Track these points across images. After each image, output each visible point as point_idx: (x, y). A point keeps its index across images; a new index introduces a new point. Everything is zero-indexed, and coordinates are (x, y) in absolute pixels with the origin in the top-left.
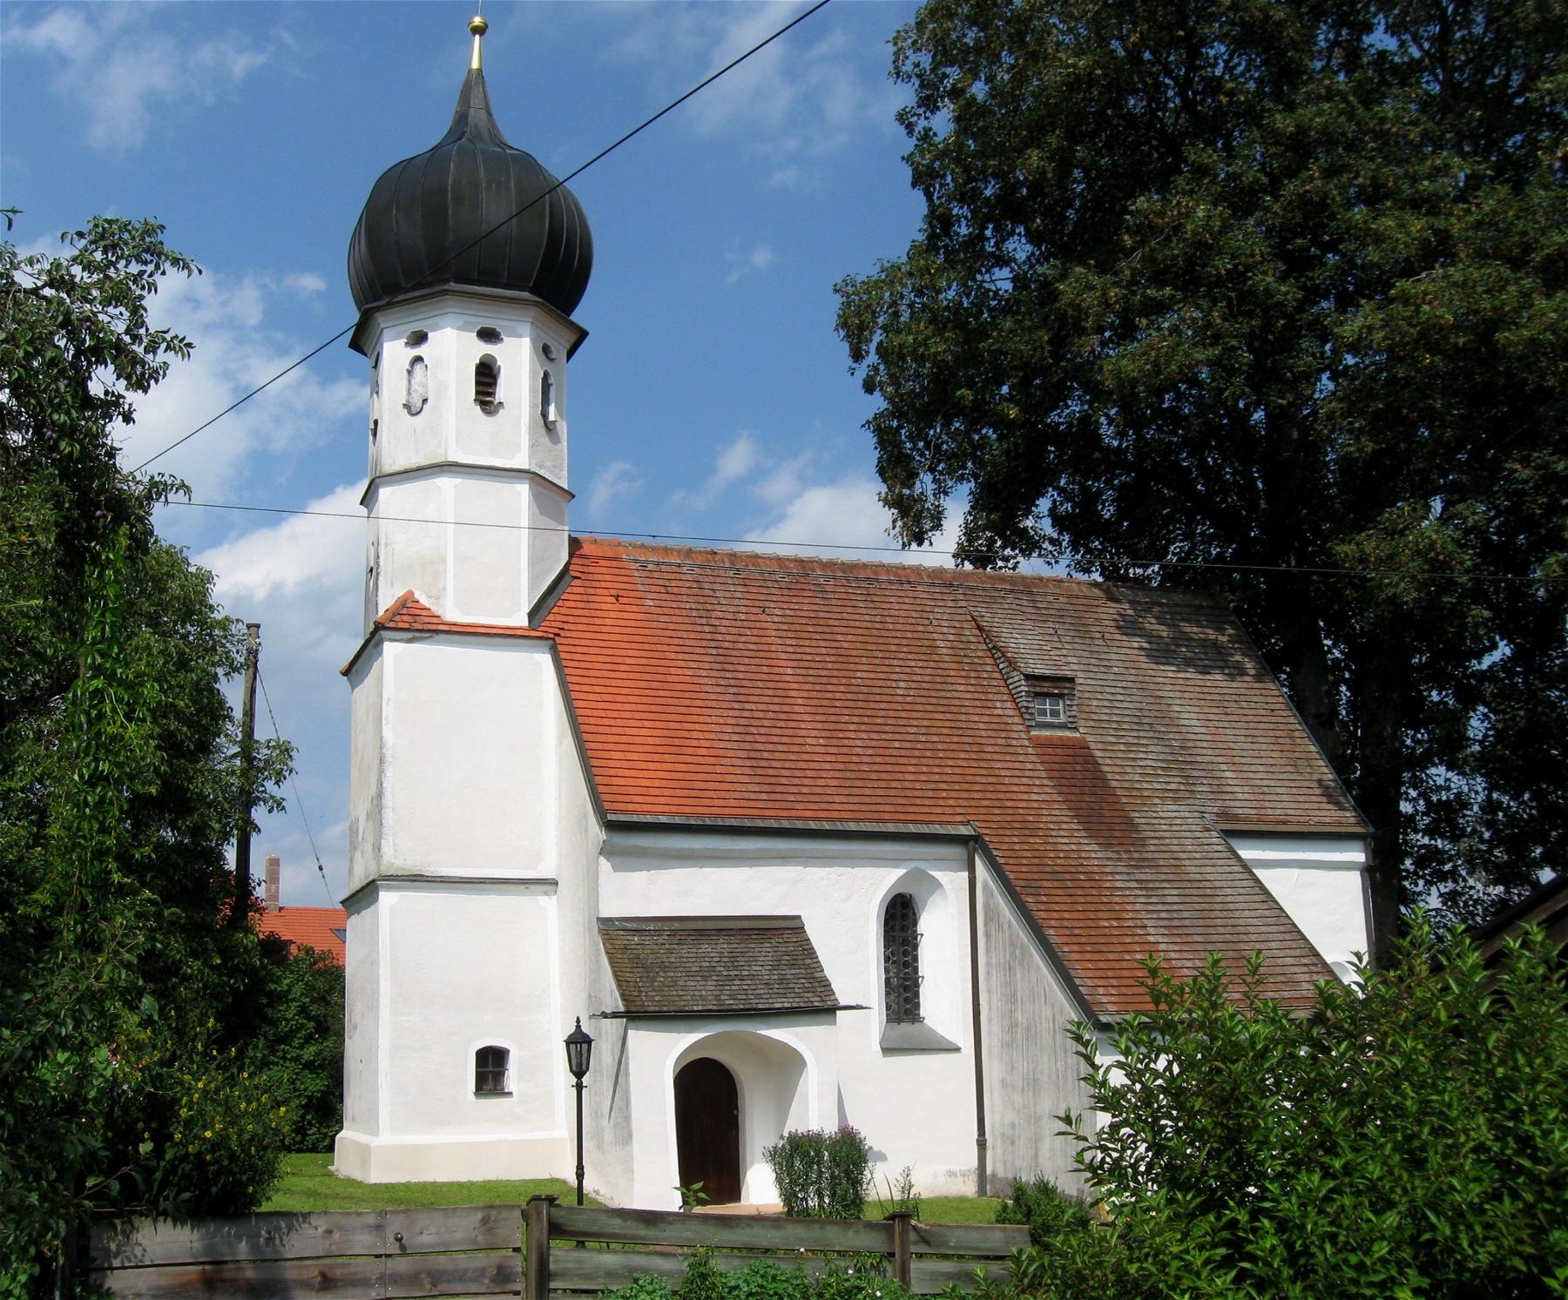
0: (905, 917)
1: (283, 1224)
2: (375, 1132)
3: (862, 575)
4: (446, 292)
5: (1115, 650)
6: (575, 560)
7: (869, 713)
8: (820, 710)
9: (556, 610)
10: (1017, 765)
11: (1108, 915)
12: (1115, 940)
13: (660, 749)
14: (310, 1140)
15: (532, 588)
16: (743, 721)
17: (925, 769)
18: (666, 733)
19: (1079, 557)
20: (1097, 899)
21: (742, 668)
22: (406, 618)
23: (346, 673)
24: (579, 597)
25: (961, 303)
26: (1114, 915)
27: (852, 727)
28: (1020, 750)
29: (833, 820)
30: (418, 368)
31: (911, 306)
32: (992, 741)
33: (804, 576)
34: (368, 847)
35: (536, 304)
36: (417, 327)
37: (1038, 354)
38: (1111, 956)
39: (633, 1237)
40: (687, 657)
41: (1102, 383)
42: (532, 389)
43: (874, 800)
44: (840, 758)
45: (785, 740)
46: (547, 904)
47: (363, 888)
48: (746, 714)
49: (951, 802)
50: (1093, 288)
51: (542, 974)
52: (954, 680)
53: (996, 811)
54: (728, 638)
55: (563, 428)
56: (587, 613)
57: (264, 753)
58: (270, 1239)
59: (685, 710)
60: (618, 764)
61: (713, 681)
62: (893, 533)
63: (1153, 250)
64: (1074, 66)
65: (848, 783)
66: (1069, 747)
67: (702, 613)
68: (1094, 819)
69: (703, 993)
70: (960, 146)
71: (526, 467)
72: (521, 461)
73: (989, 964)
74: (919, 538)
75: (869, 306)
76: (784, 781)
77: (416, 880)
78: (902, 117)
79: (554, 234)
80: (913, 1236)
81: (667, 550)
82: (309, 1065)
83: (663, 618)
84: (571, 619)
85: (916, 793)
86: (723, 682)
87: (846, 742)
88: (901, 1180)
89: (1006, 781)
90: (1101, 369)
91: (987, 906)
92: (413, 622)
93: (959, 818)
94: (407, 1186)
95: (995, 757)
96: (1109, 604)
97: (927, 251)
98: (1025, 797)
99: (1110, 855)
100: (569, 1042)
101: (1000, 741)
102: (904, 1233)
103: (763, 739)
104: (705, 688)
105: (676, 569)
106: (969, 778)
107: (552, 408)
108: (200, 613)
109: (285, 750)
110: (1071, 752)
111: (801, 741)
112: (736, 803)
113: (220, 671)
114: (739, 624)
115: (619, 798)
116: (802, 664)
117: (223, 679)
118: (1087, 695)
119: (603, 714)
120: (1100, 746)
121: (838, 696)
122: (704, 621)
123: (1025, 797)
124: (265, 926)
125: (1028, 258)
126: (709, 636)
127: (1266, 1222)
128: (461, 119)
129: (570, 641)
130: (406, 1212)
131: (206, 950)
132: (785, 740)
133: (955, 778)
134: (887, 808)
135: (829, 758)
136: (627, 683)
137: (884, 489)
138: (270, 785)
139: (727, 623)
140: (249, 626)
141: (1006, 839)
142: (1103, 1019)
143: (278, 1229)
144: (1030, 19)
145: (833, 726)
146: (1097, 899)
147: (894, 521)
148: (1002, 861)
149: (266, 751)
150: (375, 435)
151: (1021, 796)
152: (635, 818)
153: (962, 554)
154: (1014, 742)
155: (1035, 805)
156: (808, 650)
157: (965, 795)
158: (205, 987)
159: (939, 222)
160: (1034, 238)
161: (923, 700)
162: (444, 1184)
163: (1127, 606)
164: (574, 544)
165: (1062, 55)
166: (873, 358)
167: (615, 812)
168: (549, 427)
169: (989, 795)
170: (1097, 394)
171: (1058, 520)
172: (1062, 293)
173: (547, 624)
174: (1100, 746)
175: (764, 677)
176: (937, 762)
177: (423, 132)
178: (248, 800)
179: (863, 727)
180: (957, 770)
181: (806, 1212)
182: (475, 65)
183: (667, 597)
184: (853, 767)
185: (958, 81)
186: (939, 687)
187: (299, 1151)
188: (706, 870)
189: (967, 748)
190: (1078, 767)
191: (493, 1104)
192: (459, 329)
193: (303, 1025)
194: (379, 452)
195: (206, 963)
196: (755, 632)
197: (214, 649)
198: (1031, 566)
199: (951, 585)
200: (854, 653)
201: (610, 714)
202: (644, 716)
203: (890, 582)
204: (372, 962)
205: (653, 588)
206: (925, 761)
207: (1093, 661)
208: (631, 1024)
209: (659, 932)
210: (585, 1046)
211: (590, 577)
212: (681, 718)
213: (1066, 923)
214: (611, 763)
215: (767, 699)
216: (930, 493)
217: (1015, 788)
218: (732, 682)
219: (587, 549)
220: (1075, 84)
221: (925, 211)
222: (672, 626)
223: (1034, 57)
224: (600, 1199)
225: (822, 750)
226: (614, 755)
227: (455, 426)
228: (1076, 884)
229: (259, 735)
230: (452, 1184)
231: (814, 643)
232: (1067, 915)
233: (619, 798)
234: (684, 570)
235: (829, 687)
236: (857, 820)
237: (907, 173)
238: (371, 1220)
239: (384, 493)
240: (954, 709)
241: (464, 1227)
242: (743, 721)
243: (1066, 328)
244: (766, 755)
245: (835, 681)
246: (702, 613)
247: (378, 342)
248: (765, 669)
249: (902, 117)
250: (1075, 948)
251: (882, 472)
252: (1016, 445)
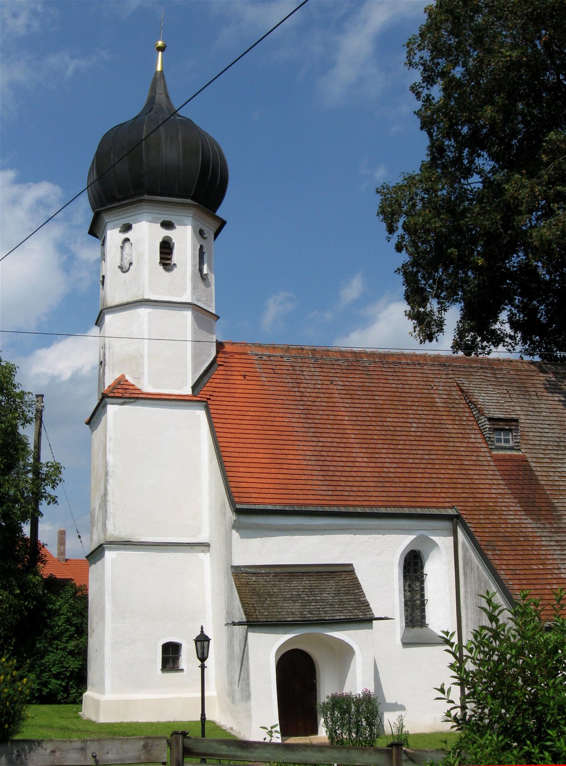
0: (416, 564)
1: (26, 747)
2: (102, 692)
3: (391, 360)
4: (141, 201)
5: (544, 402)
6: (220, 355)
7: (394, 442)
8: (365, 441)
9: (208, 384)
10: (484, 472)
11: (537, 562)
12: (541, 577)
13: (268, 466)
14: (71, 699)
15: (194, 372)
16: (318, 449)
17: (427, 475)
18: (273, 456)
19: (527, 347)
20: (531, 552)
21: (318, 417)
22: (120, 391)
23: (88, 423)
24: (222, 377)
25: (450, 198)
26: (540, 562)
27: (384, 451)
28: (485, 463)
29: (371, 506)
30: (127, 245)
31: (422, 199)
32: (468, 458)
33: (358, 362)
34: (100, 525)
35: (194, 206)
36: (126, 221)
37: (494, 227)
38: (538, 587)
39: (234, 756)
40: (285, 411)
41: (532, 243)
42: (193, 256)
43: (397, 494)
44: (376, 470)
45: (343, 459)
46: (205, 558)
47: (96, 549)
48: (320, 444)
49: (443, 495)
50: (525, 187)
51: (200, 597)
52: (446, 422)
53: (470, 500)
54: (310, 399)
55: (212, 278)
56: (227, 386)
57: (44, 470)
58: (19, 755)
59: (284, 442)
60: (243, 475)
61: (301, 425)
62: (414, 334)
63: (560, 163)
64: (510, 56)
65: (381, 484)
66: (517, 461)
67: (295, 385)
68: (530, 504)
69: (293, 610)
70: (446, 105)
71: (190, 301)
72: (187, 298)
73: (466, 592)
74: (430, 337)
75: (397, 201)
76: (342, 484)
78: (413, 89)
79: (205, 166)
80: (404, 757)
81: (274, 348)
82: (71, 653)
83: (271, 388)
84: (217, 390)
85: (422, 490)
86: (306, 425)
87: (380, 460)
88: (397, 723)
89: (477, 482)
90: (531, 234)
91: (464, 556)
92: (124, 393)
93: (447, 505)
94: (121, 724)
95: (470, 467)
96: (541, 374)
97: (430, 167)
98: (488, 491)
99: (539, 525)
100: (196, 641)
101: (473, 458)
102: (398, 755)
103: (330, 459)
104: (296, 429)
105: (279, 359)
106: (455, 481)
107: (205, 267)
108: (7, 389)
109: (57, 468)
110: (516, 464)
111: (353, 459)
112: (313, 497)
113: (19, 422)
114: (317, 391)
115: (244, 495)
116: (354, 414)
117: (20, 427)
118: (527, 429)
119: (235, 445)
120: (534, 460)
121: (375, 432)
122: (296, 389)
123: (488, 491)
124: (46, 571)
125: (491, 169)
126: (299, 398)
127: (547, 754)
128: (151, 100)
129: (217, 403)
130: (99, 740)
131: (11, 585)
132: (343, 459)
133: (446, 481)
134: (404, 499)
135: (369, 470)
136: (250, 427)
137: (408, 308)
138: (48, 489)
139: (310, 390)
140: (37, 396)
141: (476, 517)
143: (24, 750)
144: (486, 29)
145: (372, 451)
146: (531, 552)
147: (415, 327)
148: (473, 530)
149: (46, 469)
150: (103, 284)
151: (485, 491)
152: (253, 507)
153: (456, 346)
154: (482, 459)
155: (494, 496)
156: (358, 406)
157: (451, 490)
158: (10, 606)
159: (437, 150)
160: (493, 156)
161: (427, 434)
162: (142, 724)
163: (551, 375)
164: (220, 346)
165: (503, 50)
166: (400, 231)
167: (242, 503)
168: (204, 278)
169: (466, 491)
170: (528, 248)
171: (514, 324)
172: (506, 190)
173: (203, 393)
174: (534, 460)
175: (331, 422)
176: (435, 471)
178: (38, 496)
179: (391, 451)
180: (447, 476)
181: (341, 742)
182: (159, 68)
183: (275, 376)
184: (384, 475)
185: (444, 67)
186: (436, 426)
187: (66, 703)
188: (295, 537)
189: (453, 462)
190: (521, 473)
192: (150, 222)
193: (67, 630)
194: (105, 294)
195: (11, 592)
196: (327, 395)
197: (16, 409)
198: (499, 353)
199: (445, 365)
200: (386, 406)
201: (239, 445)
202: (259, 446)
203: (407, 364)
204: (102, 593)
205: (266, 371)
206: (428, 471)
207: (530, 409)
208: (250, 629)
209: (267, 574)
210: (206, 643)
211: (229, 365)
212: (281, 447)
213: (511, 567)
214: (239, 474)
215: (333, 435)
216: (435, 310)
217: (482, 486)
218: (312, 425)
219: (228, 348)
220: (513, 65)
221: (428, 143)
222: (277, 393)
223: (489, 51)
224: (233, 733)
225: (365, 465)
226: (241, 469)
227: (148, 278)
228: (518, 543)
229: (43, 460)
230: (147, 723)
231: (361, 401)
232: (512, 562)
233: (244, 495)
234: (285, 359)
235: (371, 428)
236: (386, 507)
237: (418, 122)
238: (78, 745)
239: (108, 318)
240: (446, 439)
241: (133, 750)
242: (318, 449)
243: (511, 210)
244: (332, 468)
245: (374, 424)
246: (295, 385)
247: (104, 232)
248: (332, 417)
249: (413, 89)
250: (517, 582)
251: (408, 298)
252: (484, 281)
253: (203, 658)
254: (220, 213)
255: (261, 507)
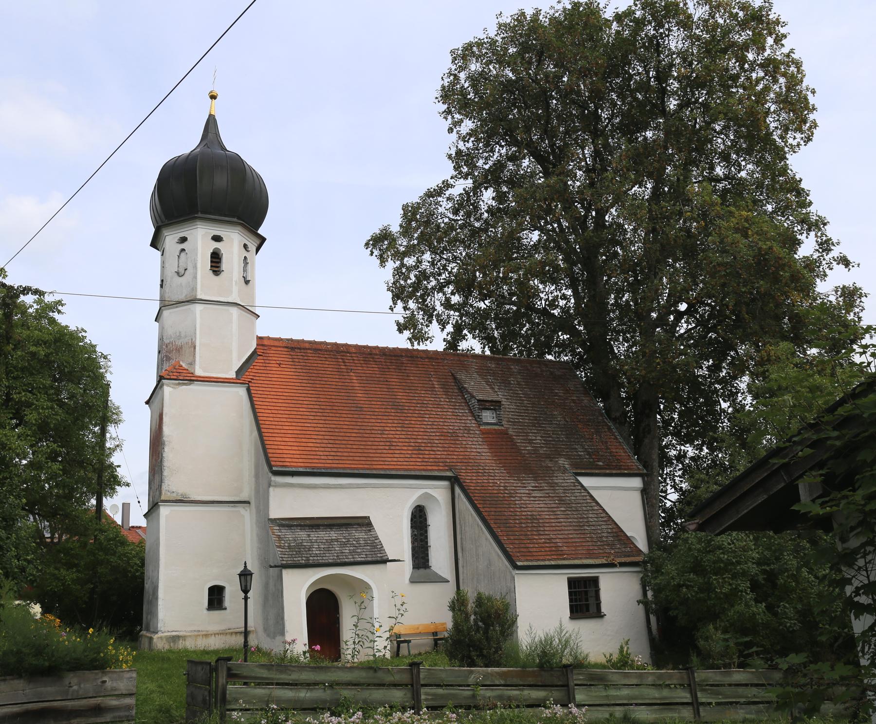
4: (196, 218)
23: (147, 403)
30: (183, 254)
36: (182, 235)
77: (181, 501)
142: (519, 564)
152: (287, 469)
167: (277, 466)
173: (245, 375)
177: (187, 143)
191: (216, 614)
253: (246, 591)
254: (260, 231)
255: (294, 469)
